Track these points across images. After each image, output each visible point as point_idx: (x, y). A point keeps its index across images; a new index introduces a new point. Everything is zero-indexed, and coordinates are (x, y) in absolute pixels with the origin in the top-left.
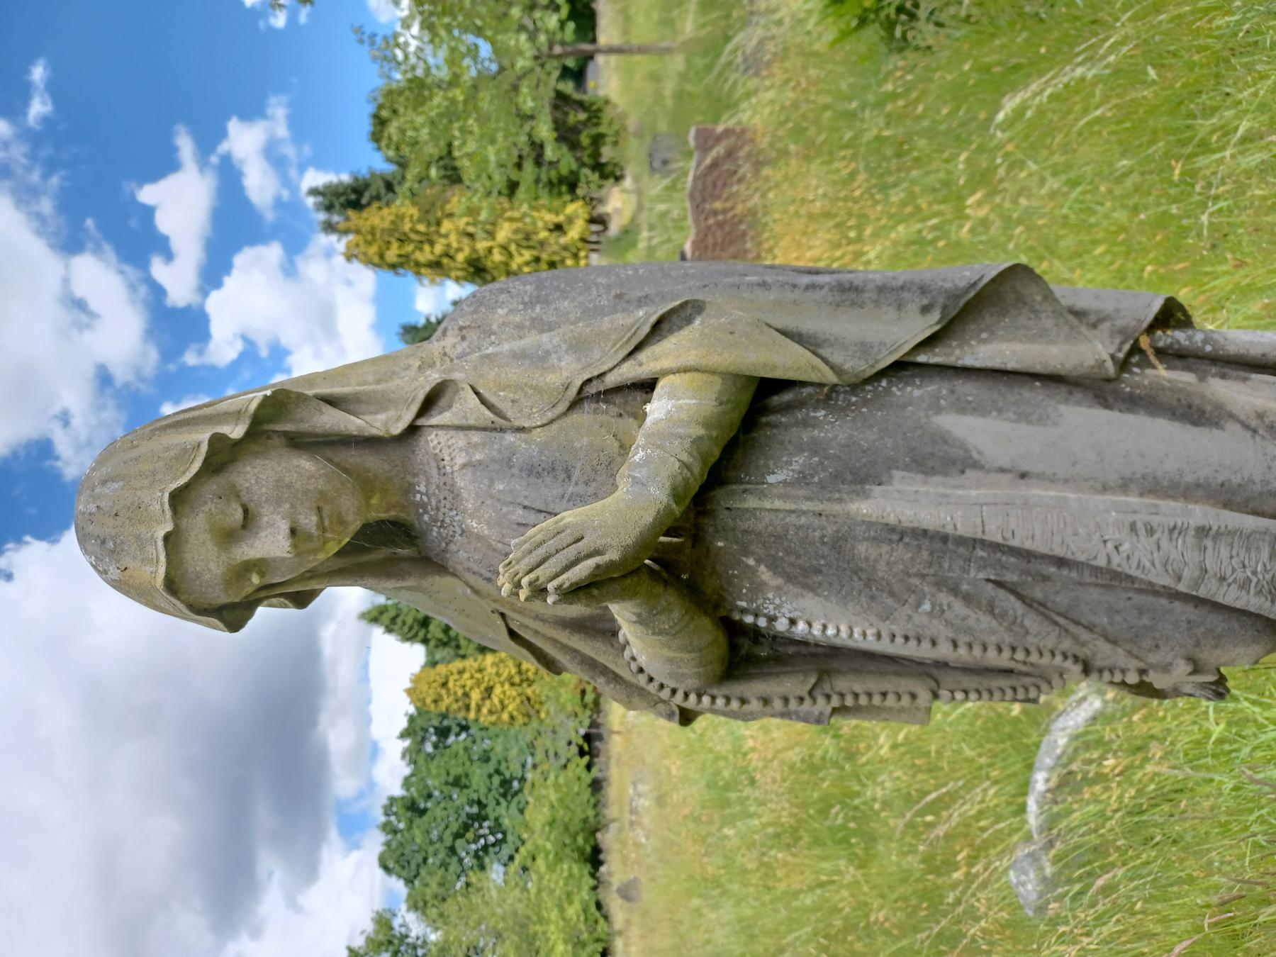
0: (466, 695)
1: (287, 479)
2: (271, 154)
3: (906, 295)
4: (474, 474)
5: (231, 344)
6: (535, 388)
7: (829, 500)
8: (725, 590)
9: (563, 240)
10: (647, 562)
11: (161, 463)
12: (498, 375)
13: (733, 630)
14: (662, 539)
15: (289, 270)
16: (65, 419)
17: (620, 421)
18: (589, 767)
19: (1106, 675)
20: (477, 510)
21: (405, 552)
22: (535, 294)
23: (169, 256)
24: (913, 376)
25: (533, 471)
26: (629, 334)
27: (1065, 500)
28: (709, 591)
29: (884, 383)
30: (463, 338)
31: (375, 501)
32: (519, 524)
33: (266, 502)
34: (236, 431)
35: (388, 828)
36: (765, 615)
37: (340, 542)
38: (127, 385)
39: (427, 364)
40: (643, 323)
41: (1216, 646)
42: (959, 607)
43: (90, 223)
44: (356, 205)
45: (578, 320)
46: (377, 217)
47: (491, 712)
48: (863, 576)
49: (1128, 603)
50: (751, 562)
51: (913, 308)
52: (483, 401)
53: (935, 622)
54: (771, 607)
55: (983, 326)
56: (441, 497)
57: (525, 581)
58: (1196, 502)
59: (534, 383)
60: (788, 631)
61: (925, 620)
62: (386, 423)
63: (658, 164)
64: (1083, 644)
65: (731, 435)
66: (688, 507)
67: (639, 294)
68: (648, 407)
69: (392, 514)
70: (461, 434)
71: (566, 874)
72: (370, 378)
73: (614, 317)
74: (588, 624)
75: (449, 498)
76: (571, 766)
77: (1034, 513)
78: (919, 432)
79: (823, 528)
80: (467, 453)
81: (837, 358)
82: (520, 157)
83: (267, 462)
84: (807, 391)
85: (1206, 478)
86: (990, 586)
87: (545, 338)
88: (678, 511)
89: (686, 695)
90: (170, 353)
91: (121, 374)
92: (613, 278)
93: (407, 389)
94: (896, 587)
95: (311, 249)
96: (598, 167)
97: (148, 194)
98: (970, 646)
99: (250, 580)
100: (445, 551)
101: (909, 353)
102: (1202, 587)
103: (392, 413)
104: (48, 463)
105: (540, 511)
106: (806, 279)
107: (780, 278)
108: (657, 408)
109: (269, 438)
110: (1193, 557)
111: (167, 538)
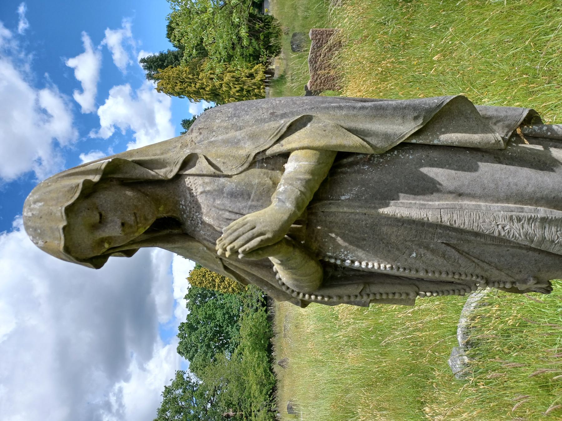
0: (213, 280)
1: (120, 201)
2: (125, 45)
3: (406, 111)
4: (206, 196)
5: (109, 129)
6: (234, 157)
7: (369, 207)
8: (322, 248)
9: (253, 81)
10: (286, 236)
11: (61, 194)
12: (216, 151)
13: (325, 265)
14: (293, 226)
15: (134, 96)
16: (39, 161)
17: (273, 172)
18: (266, 311)
19: (496, 284)
20: (208, 212)
21: (176, 231)
22: (233, 113)
23: (81, 91)
24: (410, 149)
25: (233, 195)
26: (277, 131)
27: (479, 206)
28: (314, 248)
29: (396, 153)
30: (200, 133)
31: (161, 209)
32: (227, 219)
33: (110, 211)
34: (96, 178)
35: (181, 336)
36: (340, 259)
37: (145, 228)
38: (65, 147)
39: (185, 146)
40: (283, 126)
41: (548, 271)
42: (429, 255)
43: (47, 75)
44: (162, 67)
45: (253, 125)
46: (171, 72)
47: (224, 288)
48: (385, 242)
49: (508, 252)
50: (333, 235)
51: (410, 117)
52: (210, 163)
53: (417, 262)
54: (343, 255)
55: (442, 126)
56: (192, 207)
57: (228, 248)
58: (541, 206)
59: (233, 154)
60: (350, 266)
61: (413, 261)
62: (165, 173)
63: (296, 48)
64: (486, 271)
65: (324, 178)
66: (305, 211)
67: (281, 112)
68: (286, 166)
69: (169, 214)
70: (200, 178)
71: (257, 356)
72: (158, 152)
73: (270, 123)
74: (259, 263)
75: (195, 207)
76: (259, 311)
77: (465, 212)
78: (412, 175)
79: (366, 220)
80: (203, 187)
81: (374, 141)
82: (233, 44)
83: (110, 192)
84: (359, 157)
85: (547, 195)
86: (444, 245)
87: (238, 133)
88: (299, 214)
89: (304, 295)
90: (83, 133)
91: (63, 142)
92: (270, 104)
93: (175, 157)
94: (400, 247)
95: (143, 87)
96: (268, 47)
97: (71, 63)
98: (434, 272)
99: (104, 246)
100: (194, 231)
101: (408, 139)
102: (543, 245)
103: (168, 169)
104: (33, 181)
105: (237, 213)
106: (360, 104)
107: (348, 104)
108: (290, 166)
109: (111, 181)
110: (539, 233)
111: (64, 228)
